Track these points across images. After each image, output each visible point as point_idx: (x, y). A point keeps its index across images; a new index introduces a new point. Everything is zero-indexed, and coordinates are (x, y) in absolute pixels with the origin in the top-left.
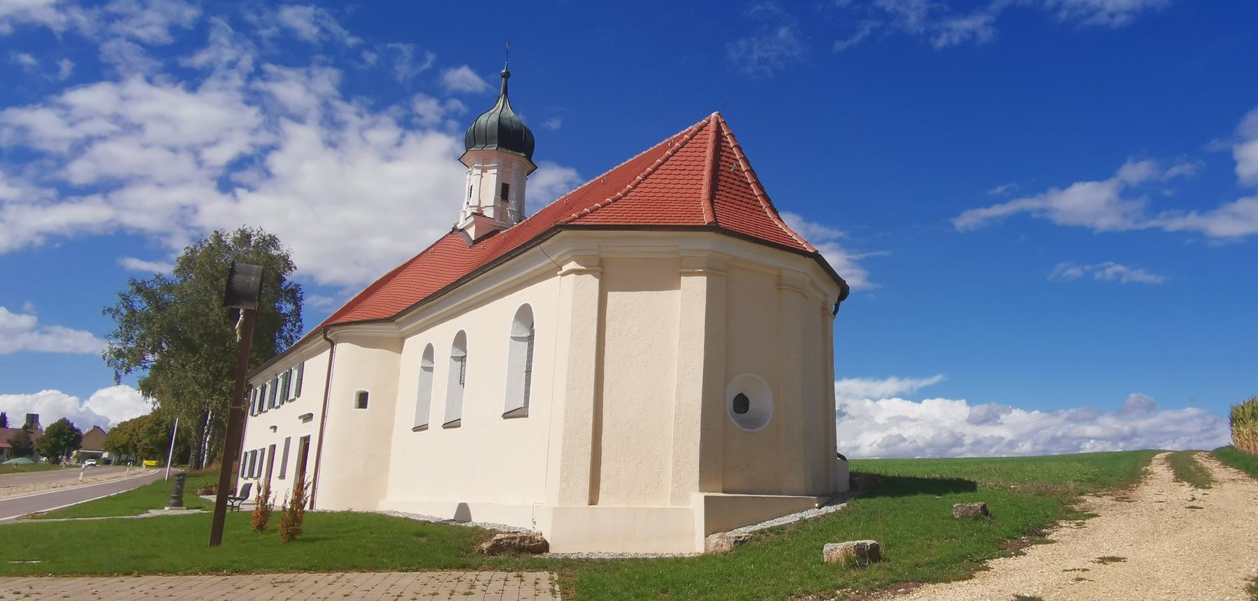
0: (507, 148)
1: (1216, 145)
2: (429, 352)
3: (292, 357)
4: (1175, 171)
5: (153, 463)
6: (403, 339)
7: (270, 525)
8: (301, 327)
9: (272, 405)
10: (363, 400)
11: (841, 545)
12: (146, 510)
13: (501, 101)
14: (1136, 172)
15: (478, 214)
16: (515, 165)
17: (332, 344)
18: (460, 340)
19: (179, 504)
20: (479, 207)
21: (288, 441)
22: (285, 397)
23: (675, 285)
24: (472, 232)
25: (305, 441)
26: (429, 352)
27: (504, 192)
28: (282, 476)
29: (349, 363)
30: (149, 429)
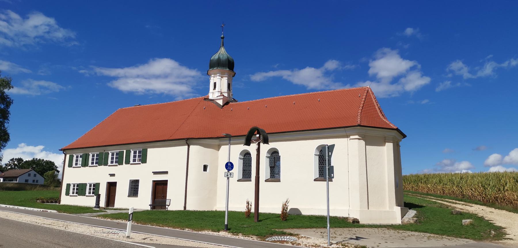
1: (364, 60)
4: (348, 67)
7: (251, 215)
9: (128, 162)
11: (469, 220)
14: (331, 65)
15: (222, 94)
23: (384, 145)
24: (221, 102)
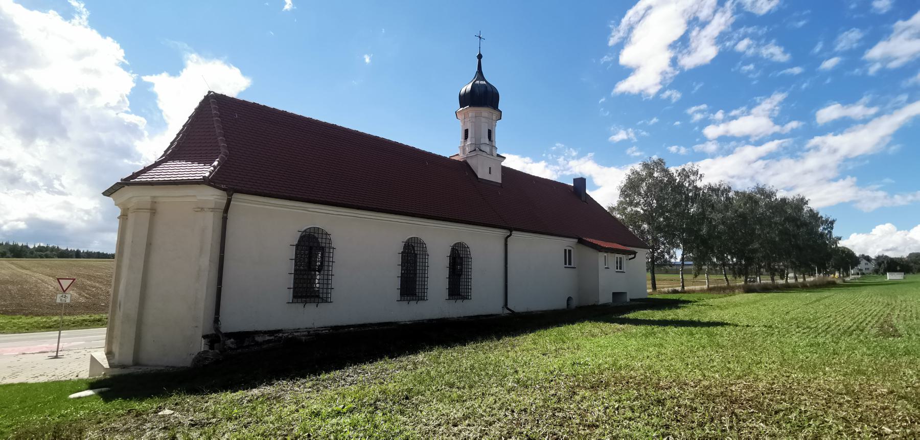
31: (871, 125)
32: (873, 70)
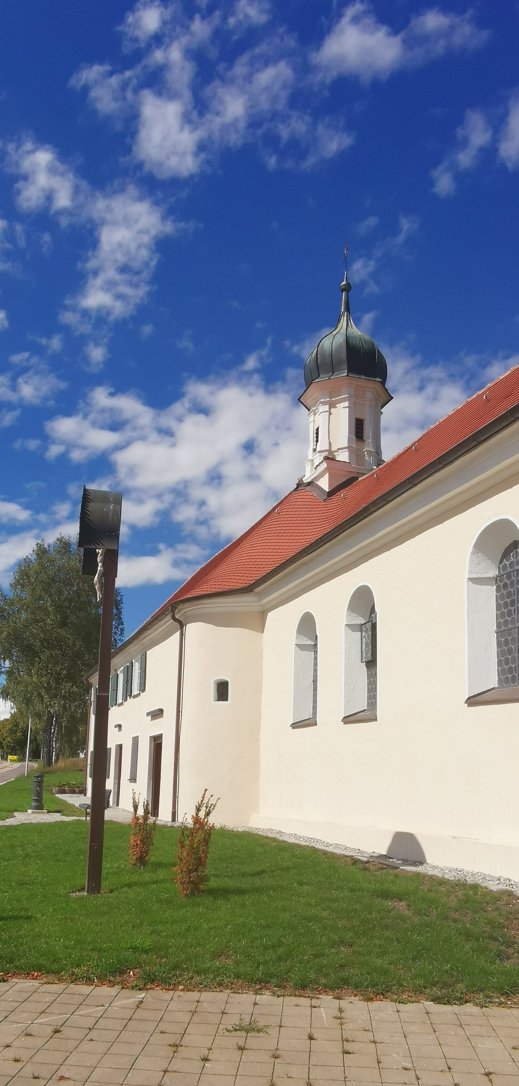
0: (359, 373)
2: (307, 625)
3: (134, 648)
5: (15, 757)
6: (263, 615)
8: (122, 630)
10: (222, 691)
12: (10, 813)
13: (344, 321)
16: (369, 395)
17: (182, 625)
18: (363, 602)
19: (39, 807)
20: (330, 451)
21: (136, 741)
22: (128, 693)
25: (157, 743)
26: (307, 625)
27: (358, 429)
28: (133, 779)
29: (204, 643)
30: (10, 729)
31: (14, 540)
32: (55, 451)
